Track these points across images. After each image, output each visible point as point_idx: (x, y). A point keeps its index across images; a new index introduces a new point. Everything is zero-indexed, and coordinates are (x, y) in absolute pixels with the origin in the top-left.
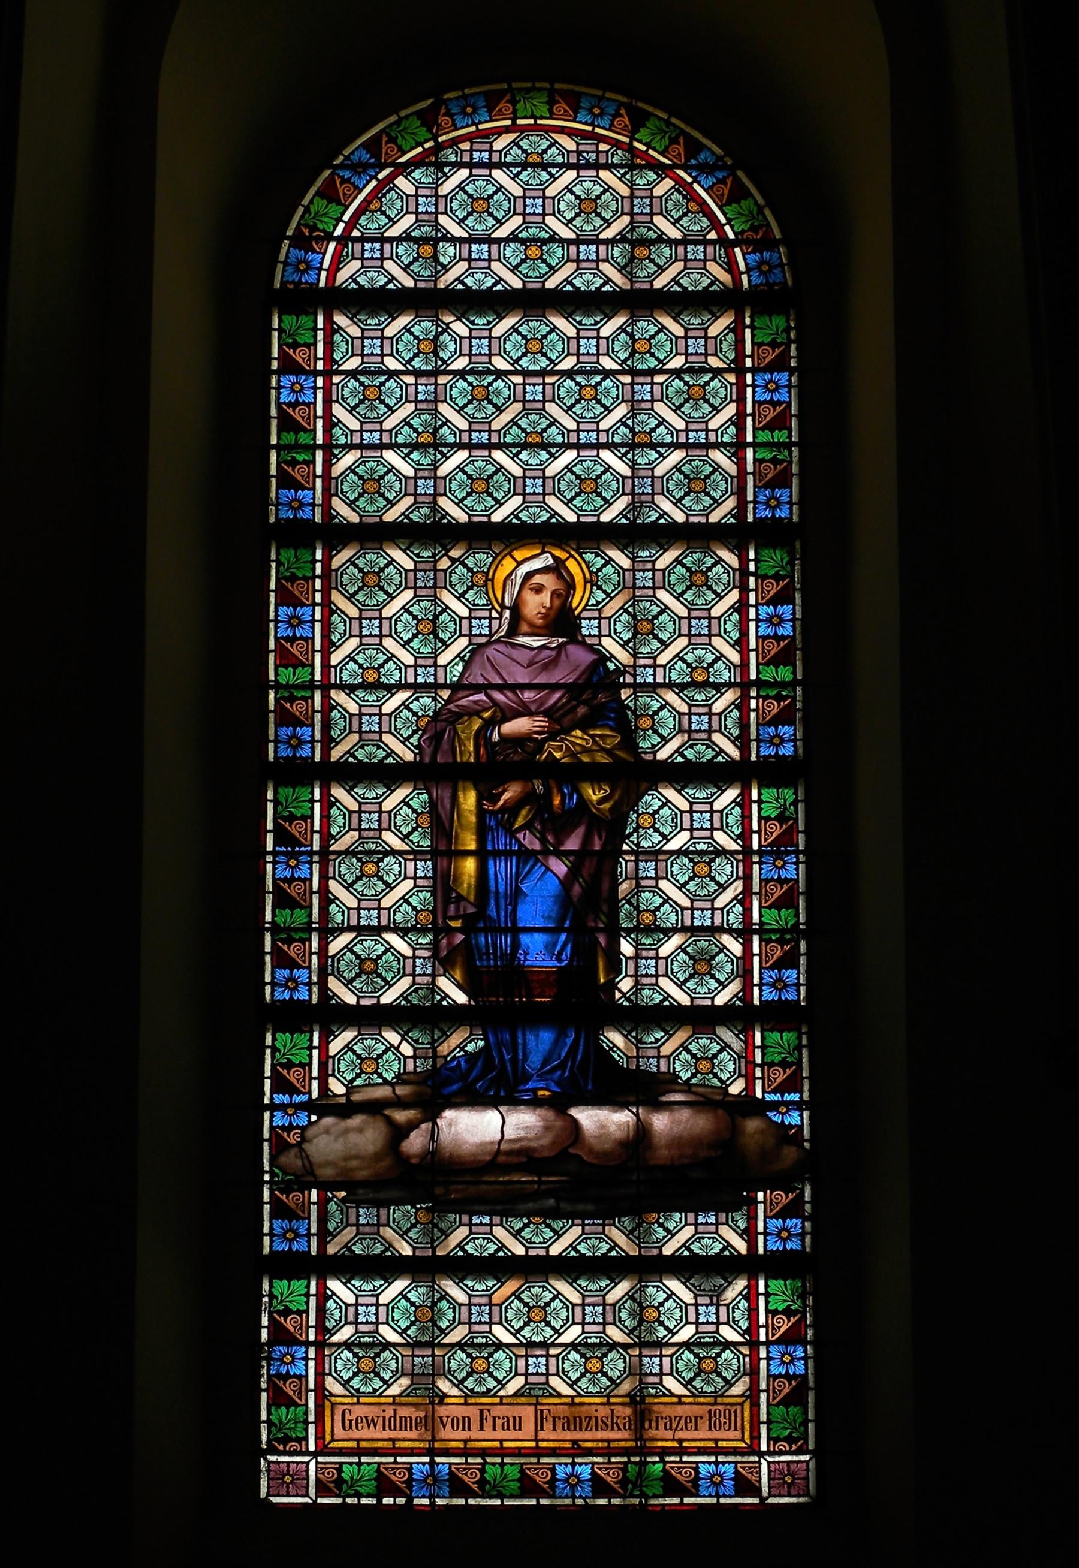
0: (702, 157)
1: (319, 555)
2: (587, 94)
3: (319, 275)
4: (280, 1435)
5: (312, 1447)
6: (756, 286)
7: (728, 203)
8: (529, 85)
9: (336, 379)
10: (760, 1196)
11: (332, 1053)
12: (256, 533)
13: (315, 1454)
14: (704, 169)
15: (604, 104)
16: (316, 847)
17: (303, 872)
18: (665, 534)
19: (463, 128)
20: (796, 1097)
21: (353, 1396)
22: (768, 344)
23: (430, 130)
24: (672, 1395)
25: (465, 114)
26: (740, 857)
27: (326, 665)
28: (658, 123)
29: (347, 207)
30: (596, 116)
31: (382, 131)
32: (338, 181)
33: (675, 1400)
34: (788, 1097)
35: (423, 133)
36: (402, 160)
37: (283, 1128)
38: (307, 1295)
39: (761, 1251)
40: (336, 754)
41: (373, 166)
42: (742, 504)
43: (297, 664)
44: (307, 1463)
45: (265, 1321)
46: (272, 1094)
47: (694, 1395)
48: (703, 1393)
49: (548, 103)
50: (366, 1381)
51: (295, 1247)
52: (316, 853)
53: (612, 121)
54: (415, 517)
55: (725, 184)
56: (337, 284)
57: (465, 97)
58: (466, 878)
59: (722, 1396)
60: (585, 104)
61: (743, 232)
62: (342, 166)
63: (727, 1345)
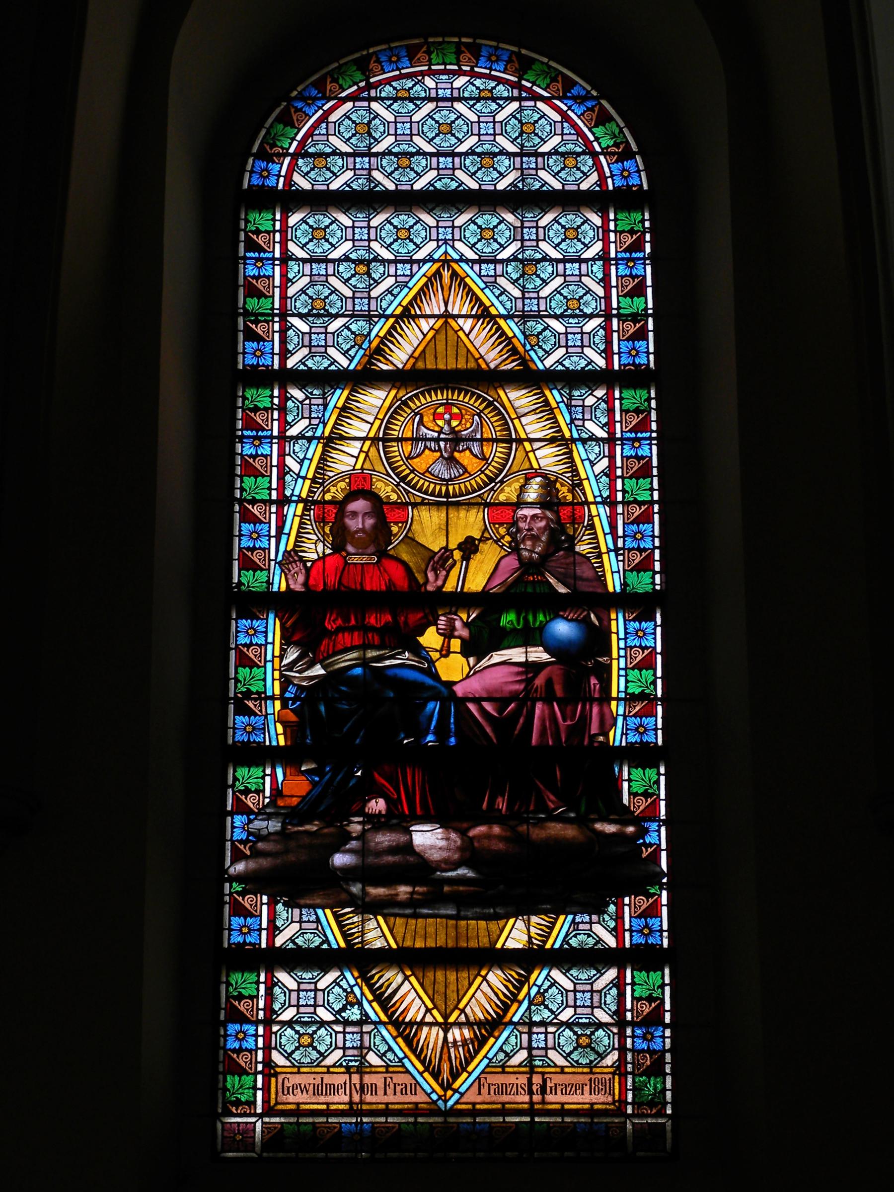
0: (575, 91)
1: (278, 217)
2: (486, 45)
3: (278, 180)
4: (236, 994)
5: (259, 1111)
6: (625, 365)
7: (596, 126)
8: (440, 39)
9: (275, 1028)
10: (626, 900)
11: (290, 224)
12: (225, 381)
13: (261, 1116)
14: (580, 100)
15: (499, 52)
16: (275, 433)
17: (265, 450)
18: (545, 200)
19: (389, 72)
20: (641, 255)
21: (294, 1066)
22: (641, 795)
23: (363, 73)
24: (556, 1066)
25: (391, 62)
26: (615, 1030)
27: (284, 297)
28: (541, 66)
29: (299, 130)
30: (492, 62)
31: (328, 73)
32: (293, 110)
33: (558, 1070)
34: (634, 255)
35: (358, 76)
36: (343, 95)
37: (248, 549)
38: (255, 1088)
39: (627, 945)
40: (290, 363)
41: (320, 99)
42: (602, 178)
43: (259, 295)
44: (255, 1123)
45: (240, 415)
46: (240, 523)
47: (573, 1066)
48: (580, 1065)
49: (455, 53)
50: (318, 293)
51: (249, 939)
52: (275, 437)
53: (506, 66)
54: (355, 186)
55: (594, 112)
56: (289, 319)
57: (391, 49)
58: (387, 893)
59: (595, 1066)
60: (484, 53)
61: (608, 147)
62: (296, 98)
63: (600, 1025)
